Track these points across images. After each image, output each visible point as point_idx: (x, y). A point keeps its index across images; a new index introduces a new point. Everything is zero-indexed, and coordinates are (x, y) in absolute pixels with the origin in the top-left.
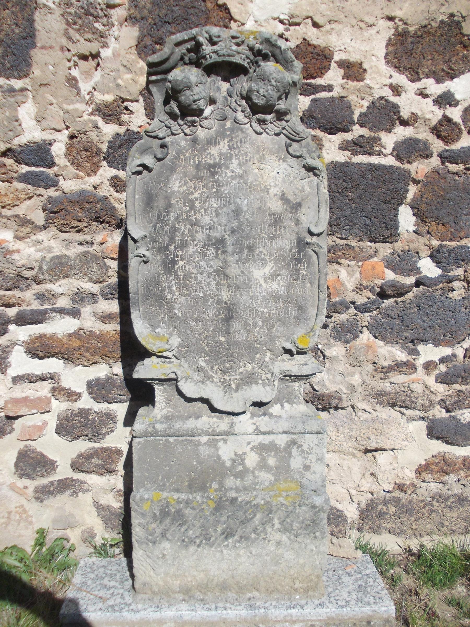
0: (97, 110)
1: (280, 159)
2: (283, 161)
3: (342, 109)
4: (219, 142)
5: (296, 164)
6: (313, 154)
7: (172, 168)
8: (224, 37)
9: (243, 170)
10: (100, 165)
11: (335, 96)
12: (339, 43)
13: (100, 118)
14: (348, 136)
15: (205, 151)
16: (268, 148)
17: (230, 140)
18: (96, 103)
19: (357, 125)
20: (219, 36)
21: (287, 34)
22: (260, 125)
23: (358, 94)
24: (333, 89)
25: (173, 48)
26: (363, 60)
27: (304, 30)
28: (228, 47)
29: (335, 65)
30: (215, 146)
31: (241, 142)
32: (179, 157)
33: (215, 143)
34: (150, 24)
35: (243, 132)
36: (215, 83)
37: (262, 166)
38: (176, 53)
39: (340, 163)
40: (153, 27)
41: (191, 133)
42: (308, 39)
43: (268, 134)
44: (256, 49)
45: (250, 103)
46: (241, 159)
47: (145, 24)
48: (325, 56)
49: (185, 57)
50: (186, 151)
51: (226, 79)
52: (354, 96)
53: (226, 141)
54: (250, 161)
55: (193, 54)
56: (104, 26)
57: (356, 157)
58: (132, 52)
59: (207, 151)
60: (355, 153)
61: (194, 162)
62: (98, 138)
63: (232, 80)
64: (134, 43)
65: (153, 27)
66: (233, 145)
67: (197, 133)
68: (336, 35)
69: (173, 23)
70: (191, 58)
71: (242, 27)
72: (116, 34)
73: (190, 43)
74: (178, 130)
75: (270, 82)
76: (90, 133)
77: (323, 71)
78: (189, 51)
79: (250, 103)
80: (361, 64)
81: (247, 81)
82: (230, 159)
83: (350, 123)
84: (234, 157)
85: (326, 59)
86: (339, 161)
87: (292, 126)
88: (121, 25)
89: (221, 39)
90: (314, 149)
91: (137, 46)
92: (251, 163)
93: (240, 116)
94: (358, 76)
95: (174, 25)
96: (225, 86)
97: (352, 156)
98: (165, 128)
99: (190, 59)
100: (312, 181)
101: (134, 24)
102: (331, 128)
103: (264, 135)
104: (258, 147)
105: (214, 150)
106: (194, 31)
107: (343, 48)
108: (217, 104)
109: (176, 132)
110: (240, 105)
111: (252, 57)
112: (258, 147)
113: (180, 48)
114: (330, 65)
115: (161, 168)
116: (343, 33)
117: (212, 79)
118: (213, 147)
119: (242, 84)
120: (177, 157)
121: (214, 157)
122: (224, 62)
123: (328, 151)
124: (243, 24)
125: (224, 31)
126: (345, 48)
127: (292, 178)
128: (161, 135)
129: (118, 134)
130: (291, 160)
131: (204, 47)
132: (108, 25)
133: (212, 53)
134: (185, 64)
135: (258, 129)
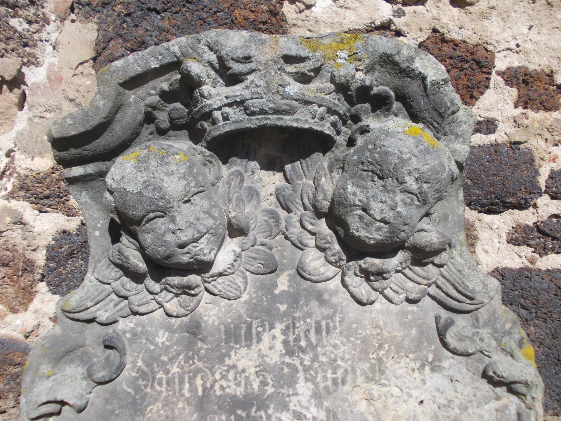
0: (21, 188)
1: (423, 366)
2: (433, 370)
3: (515, 166)
4: (258, 333)
5: (464, 371)
6: (506, 339)
7: (134, 402)
8: (263, 58)
9: (328, 411)
10: (34, 290)
11: (500, 141)
12: (505, 35)
13: (26, 204)
14: (527, 217)
15: (221, 359)
16: (391, 340)
17: (287, 327)
18: (19, 176)
19: (546, 196)
20: (247, 59)
21: (399, 23)
22: (368, 280)
23: (547, 135)
24: (496, 126)
25: (119, 95)
26: (554, 69)
27: (435, 12)
28: (274, 86)
29: (500, 79)
30: (249, 347)
31: (318, 331)
32: (153, 373)
33: (249, 337)
34: (119, 15)
35: (322, 302)
36: (242, 181)
37: (376, 390)
38: (130, 105)
39: (511, 270)
40: (125, 21)
41: (182, 311)
42: (441, 30)
43: (390, 301)
44: (355, 86)
45: (341, 232)
46: (319, 379)
47: (111, 16)
48: (478, 63)
49: (157, 114)
50: (172, 360)
51: (271, 165)
52: (539, 139)
53: (277, 331)
54: (344, 382)
55: (178, 105)
56: (30, 23)
57: (545, 257)
58: (86, 72)
59: (227, 361)
60: (543, 251)
61: (193, 389)
62: (25, 242)
63: (288, 167)
64: (88, 53)
65: (125, 21)
66: (297, 340)
67: (200, 309)
68: (499, 19)
69: (166, 11)
70: (175, 115)
71: (307, 12)
72: (54, 37)
73: (167, 76)
74: (147, 303)
75: (401, 182)
76: (8, 233)
77: (475, 94)
78: (167, 97)
79: (341, 232)
80: (551, 75)
81: (331, 171)
82: (292, 381)
83: (530, 193)
84: (301, 375)
85: (481, 67)
86: (509, 266)
87: (456, 277)
88: (63, 20)
89: (253, 66)
90: (508, 326)
91: (94, 59)
92: (347, 387)
93: (314, 261)
94: (547, 101)
95: (168, 14)
96: (271, 181)
97: (536, 255)
98: (113, 296)
99: (172, 120)
100: (506, 407)
101: (87, 18)
102: (492, 204)
103: (380, 304)
104: (364, 340)
105: (244, 358)
106: (176, 45)
107: (512, 45)
108: (251, 234)
109: (142, 309)
110: (313, 233)
111: (343, 107)
112: (364, 340)
113: (141, 91)
114: (488, 79)
115: (107, 401)
116: (513, 14)
117: (235, 168)
118: (244, 351)
119: (320, 177)
120: (147, 376)
121: (247, 378)
122: (263, 129)
123: (486, 247)
124: (309, 7)
125: (263, 42)
126: (518, 46)
127: (457, 411)
128: (103, 316)
129: (64, 232)
130: (449, 361)
131: (206, 89)
132: (36, 22)
133: (230, 105)
134: (162, 132)
135: (363, 289)
